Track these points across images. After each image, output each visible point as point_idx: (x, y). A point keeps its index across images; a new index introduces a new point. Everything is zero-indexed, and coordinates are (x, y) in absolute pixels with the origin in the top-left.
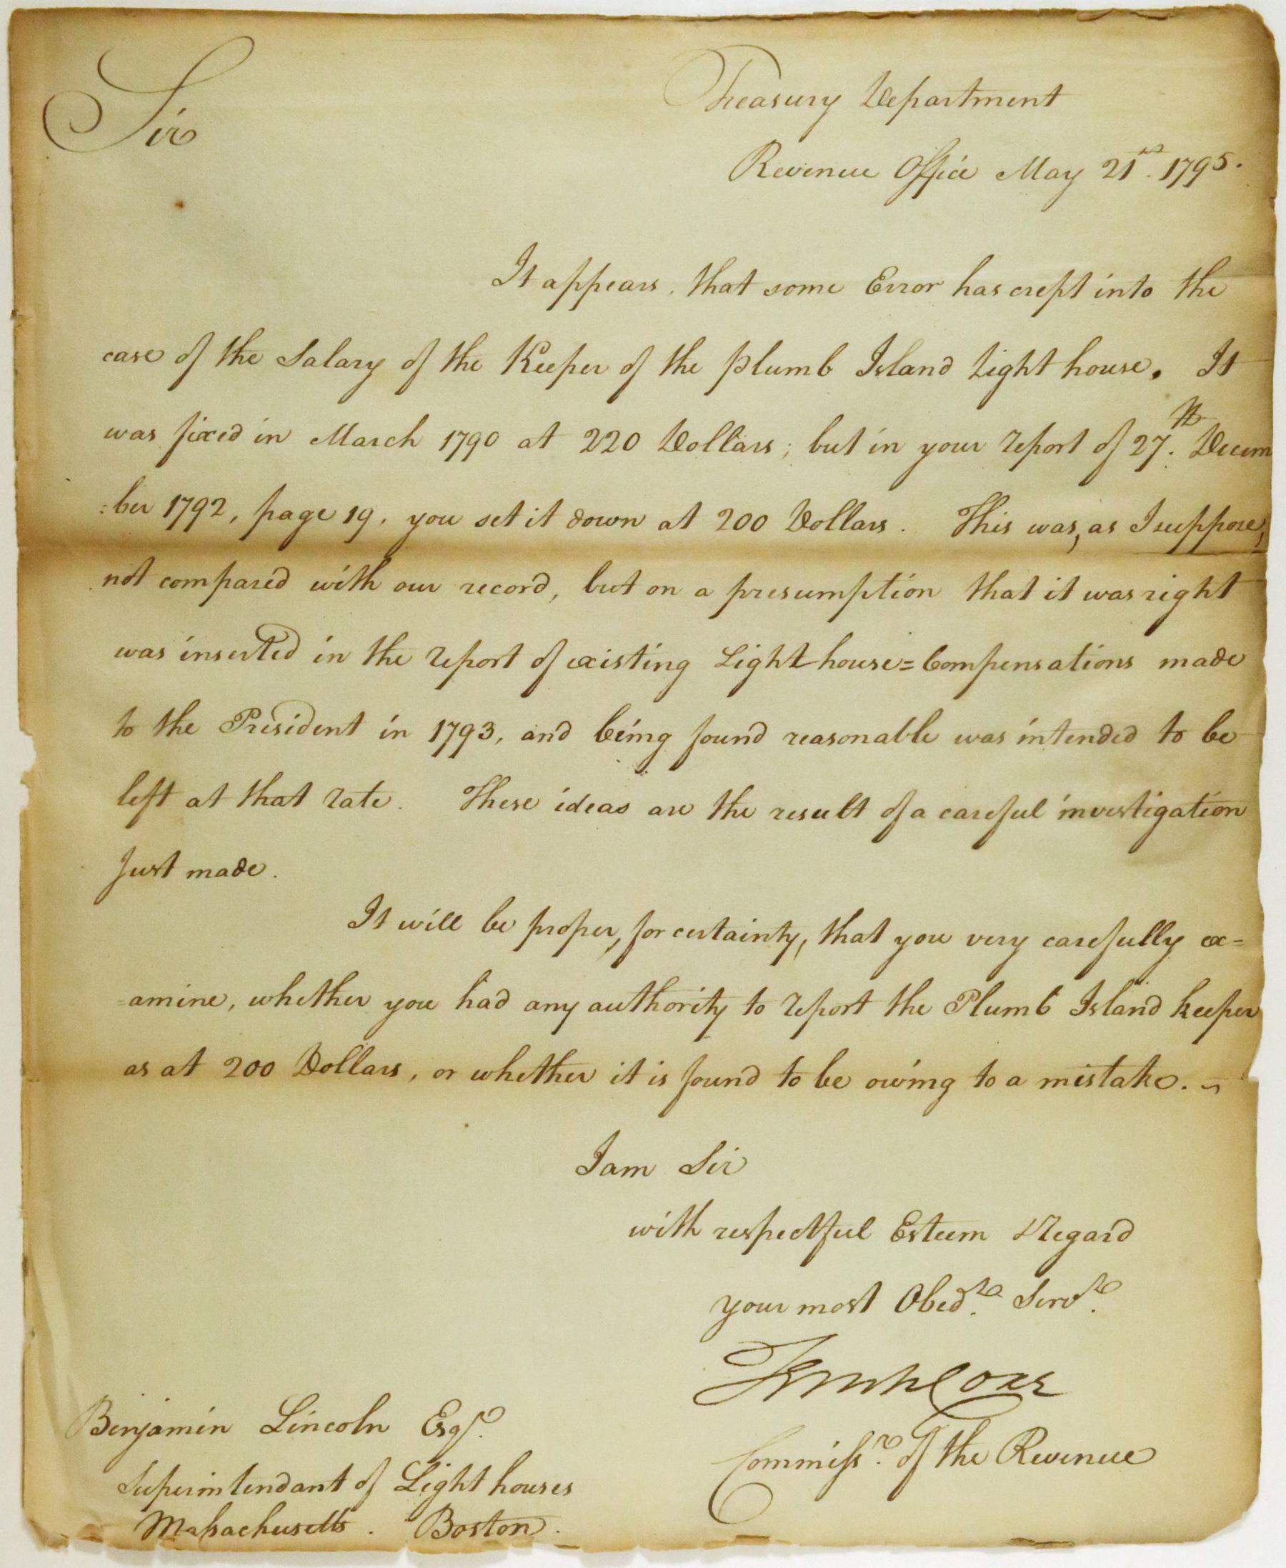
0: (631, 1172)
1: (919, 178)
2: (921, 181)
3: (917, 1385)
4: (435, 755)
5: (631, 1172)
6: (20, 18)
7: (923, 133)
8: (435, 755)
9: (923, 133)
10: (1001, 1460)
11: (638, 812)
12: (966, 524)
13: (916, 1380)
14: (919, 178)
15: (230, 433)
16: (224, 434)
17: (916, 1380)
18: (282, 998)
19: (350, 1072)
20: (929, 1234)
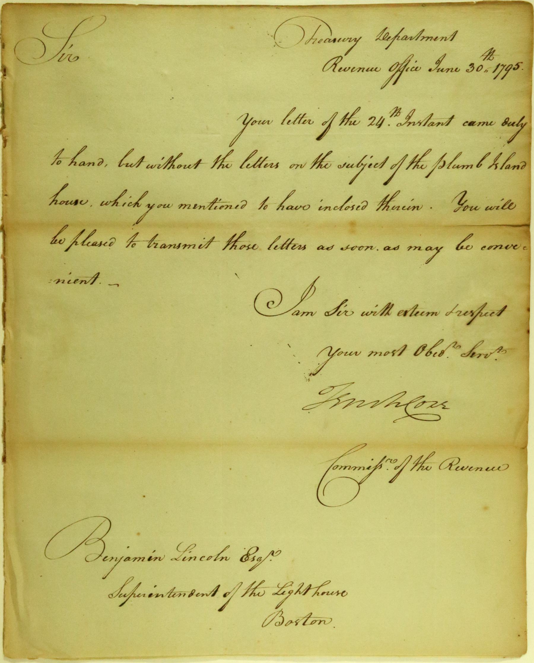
0: (183, 206)
1: (399, 70)
2: (399, 73)
3: (400, 405)
4: (495, 78)
5: (183, 206)
6: (7, 655)
7: (400, 51)
8: (495, 78)
9: (400, 51)
10: (256, 549)
11: (337, 249)
12: (394, 75)
13: (399, 403)
14: (399, 70)
15: (362, 206)
16: (359, 207)
17: (399, 403)
18: (281, 206)
19: (87, 245)
20: (502, 167)
